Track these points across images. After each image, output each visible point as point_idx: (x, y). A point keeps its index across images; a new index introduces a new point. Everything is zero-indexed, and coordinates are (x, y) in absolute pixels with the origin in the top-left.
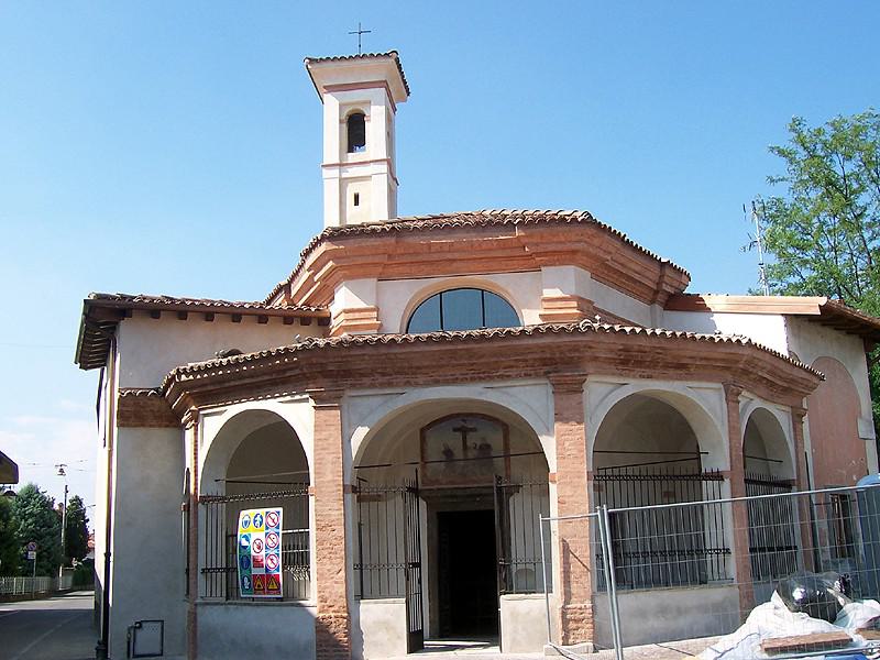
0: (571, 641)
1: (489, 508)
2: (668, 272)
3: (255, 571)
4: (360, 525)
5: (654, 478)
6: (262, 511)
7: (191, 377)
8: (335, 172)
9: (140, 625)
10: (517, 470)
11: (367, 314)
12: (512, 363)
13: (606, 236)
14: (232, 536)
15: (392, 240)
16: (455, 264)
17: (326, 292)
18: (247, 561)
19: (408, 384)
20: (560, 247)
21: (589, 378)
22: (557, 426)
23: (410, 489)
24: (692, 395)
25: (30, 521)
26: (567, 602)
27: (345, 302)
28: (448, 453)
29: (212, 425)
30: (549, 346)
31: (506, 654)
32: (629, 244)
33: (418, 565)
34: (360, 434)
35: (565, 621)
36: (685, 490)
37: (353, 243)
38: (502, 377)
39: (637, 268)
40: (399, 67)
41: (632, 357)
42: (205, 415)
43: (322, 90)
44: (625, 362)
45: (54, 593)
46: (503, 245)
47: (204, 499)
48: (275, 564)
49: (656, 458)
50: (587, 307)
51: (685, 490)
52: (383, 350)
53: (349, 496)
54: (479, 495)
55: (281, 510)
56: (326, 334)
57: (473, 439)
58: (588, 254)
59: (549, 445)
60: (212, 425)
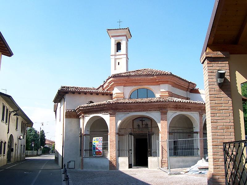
0: (163, 167)
1: (146, 138)
2: (191, 84)
3: (96, 151)
4: (119, 141)
5: (187, 133)
6: (98, 138)
7: (83, 108)
8: (114, 57)
9: (70, 162)
10: (153, 130)
11: (121, 94)
12: (152, 108)
13: (175, 78)
14: (91, 143)
15: (127, 78)
16: (141, 83)
17: (112, 88)
18: (95, 148)
19: (130, 111)
20: (164, 80)
21: (169, 111)
22: (161, 121)
23: (130, 134)
24: (191, 115)
25: (32, 136)
26: (162, 159)
27: (116, 91)
28: (139, 126)
29: (87, 118)
30: (160, 104)
31: (149, 169)
32: (181, 79)
33: (131, 150)
34: (119, 122)
35: (162, 163)
37: (118, 78)
38: (150, 111)
39: (183, 84)
40: (129, 31)
41: (177, 107)
42: (86, 116)
43: (111, 37)
44: (176, 108)
45: (37, 155)
46: (152, 79)
47: (85, 135)
48: (100, 148)
49: (181, 128)
50: (171, 95)
52: (125, 104)
53: (117, 135)
54: (145, 135)
55: (102, 138)
56: (112, 99)
57: (144, 123)
58: (171, 82)
59: (159, 125)
60: (87, 118)
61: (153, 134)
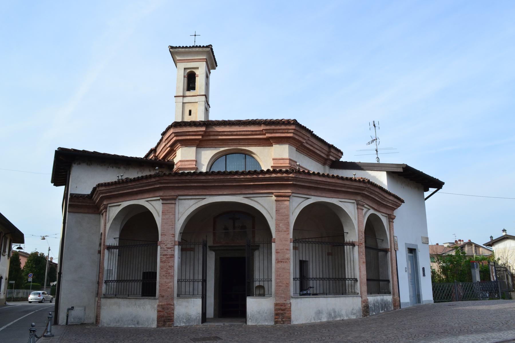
2: (332, 150)
17: (172, 151)
29: (114, 211)
36: (372, 277)
51: (372, 277)
60: (114, 211)
61: (257, 247)
